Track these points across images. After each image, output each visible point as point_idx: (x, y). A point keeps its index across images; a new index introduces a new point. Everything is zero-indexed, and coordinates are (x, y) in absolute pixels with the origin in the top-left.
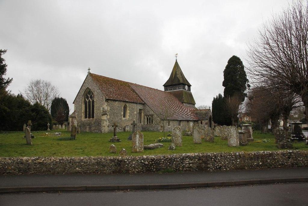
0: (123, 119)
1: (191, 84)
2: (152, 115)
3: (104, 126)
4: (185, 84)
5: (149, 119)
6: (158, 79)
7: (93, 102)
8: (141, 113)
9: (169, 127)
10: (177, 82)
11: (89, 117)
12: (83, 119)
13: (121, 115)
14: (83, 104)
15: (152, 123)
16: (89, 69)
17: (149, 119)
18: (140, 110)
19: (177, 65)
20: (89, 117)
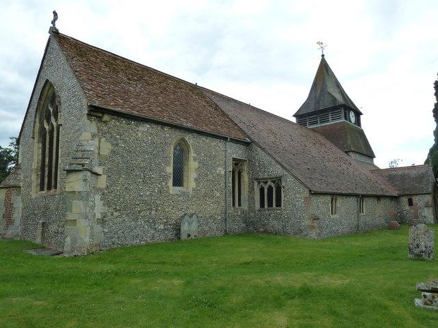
0: (173, 190)
1: (361, 110)
2: (278, 181)
4: (348, 107)
5: (266, 190)
6: (284, 98)
8: (240, 173)
9: (335, 216)
10: (330, 110)
11: (49, 188)
13: (165, 178)
14: (36, 139)
15: (279, 204)
17: (266, 190)
18: (237, 162)
19: (324, 68)
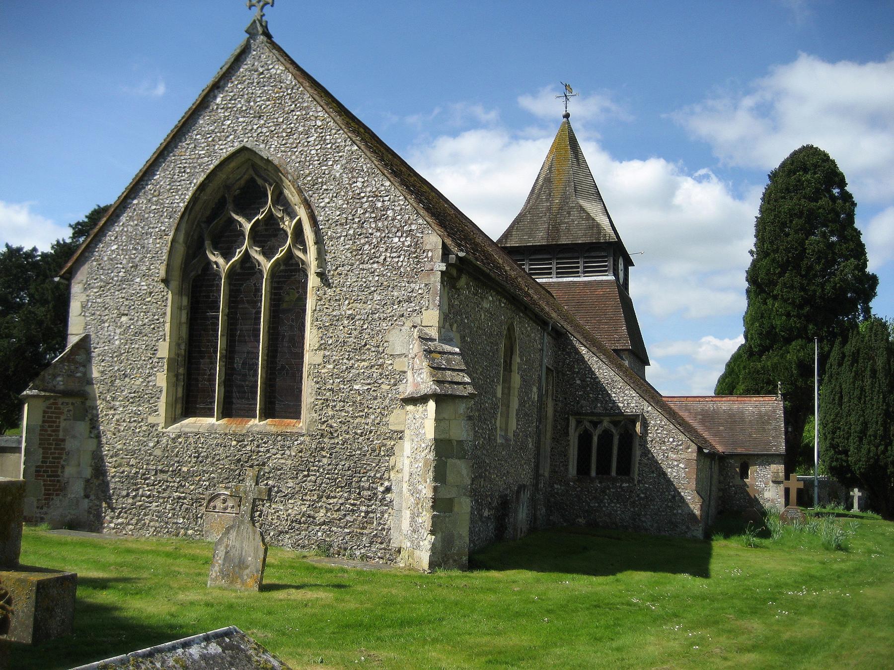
5: (595, 439)
7: (290, 274)
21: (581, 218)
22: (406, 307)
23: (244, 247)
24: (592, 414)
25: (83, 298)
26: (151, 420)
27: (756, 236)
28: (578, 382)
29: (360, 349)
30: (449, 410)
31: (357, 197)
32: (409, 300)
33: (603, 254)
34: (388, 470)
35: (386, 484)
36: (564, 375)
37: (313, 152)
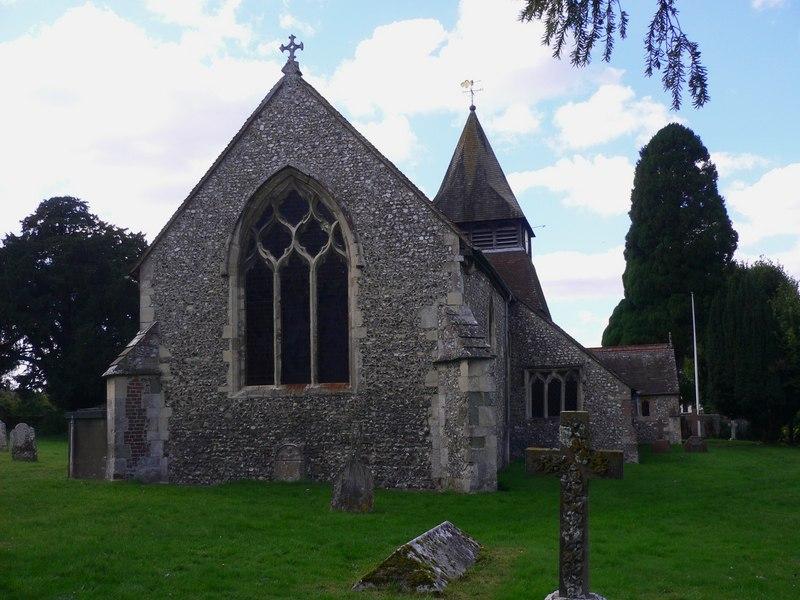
3: (481, 441)
5: (546, 387)
7: (334, 272)
11: (295, 375)
12: (235, 391)
14: (232, 279)
15: (572, 404)
16: (293, 46)
19: (474, 135)
20: (295, 375)
21: (492, 198)
22: (435, 291)
23: (291, 247)
24: (543, 367)
25: (152, 292)
26: (221, 389)
27: (632, 199)
28: (530, 341)
29: (397, 325)
30: (478, 369)
31: (387, 206)
32: (435, 285)
33: (513, 229)
34: (427, 418)
35: (426, 429)
36: (518, 335)
37: (347, 169)
